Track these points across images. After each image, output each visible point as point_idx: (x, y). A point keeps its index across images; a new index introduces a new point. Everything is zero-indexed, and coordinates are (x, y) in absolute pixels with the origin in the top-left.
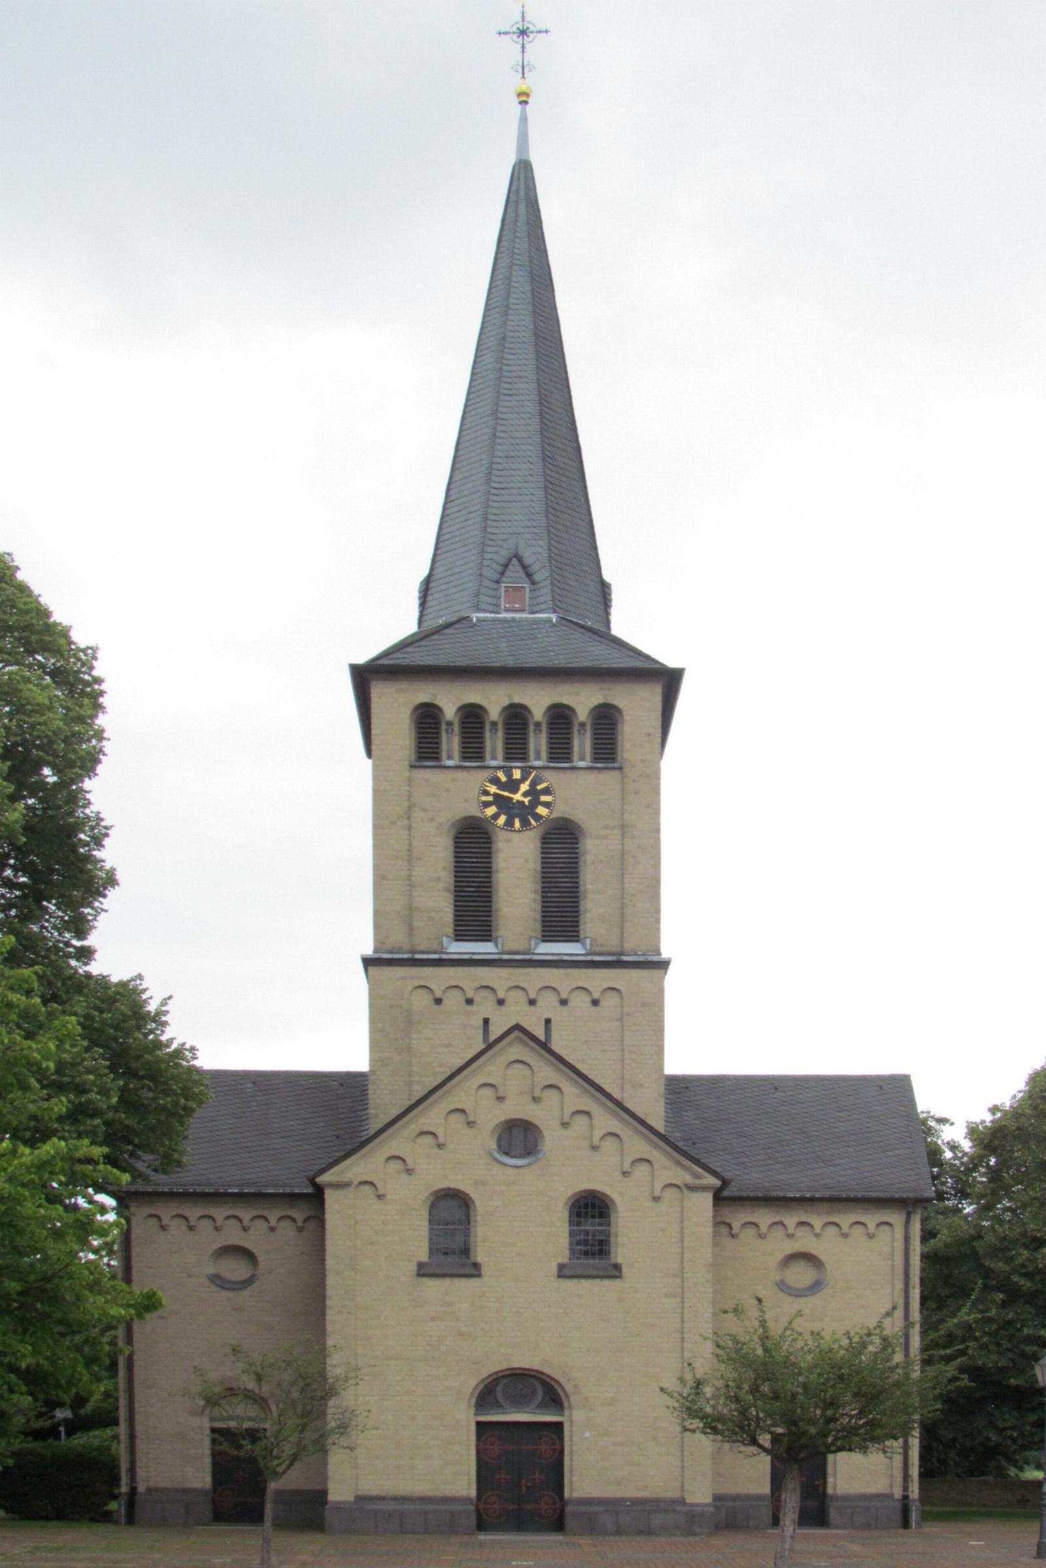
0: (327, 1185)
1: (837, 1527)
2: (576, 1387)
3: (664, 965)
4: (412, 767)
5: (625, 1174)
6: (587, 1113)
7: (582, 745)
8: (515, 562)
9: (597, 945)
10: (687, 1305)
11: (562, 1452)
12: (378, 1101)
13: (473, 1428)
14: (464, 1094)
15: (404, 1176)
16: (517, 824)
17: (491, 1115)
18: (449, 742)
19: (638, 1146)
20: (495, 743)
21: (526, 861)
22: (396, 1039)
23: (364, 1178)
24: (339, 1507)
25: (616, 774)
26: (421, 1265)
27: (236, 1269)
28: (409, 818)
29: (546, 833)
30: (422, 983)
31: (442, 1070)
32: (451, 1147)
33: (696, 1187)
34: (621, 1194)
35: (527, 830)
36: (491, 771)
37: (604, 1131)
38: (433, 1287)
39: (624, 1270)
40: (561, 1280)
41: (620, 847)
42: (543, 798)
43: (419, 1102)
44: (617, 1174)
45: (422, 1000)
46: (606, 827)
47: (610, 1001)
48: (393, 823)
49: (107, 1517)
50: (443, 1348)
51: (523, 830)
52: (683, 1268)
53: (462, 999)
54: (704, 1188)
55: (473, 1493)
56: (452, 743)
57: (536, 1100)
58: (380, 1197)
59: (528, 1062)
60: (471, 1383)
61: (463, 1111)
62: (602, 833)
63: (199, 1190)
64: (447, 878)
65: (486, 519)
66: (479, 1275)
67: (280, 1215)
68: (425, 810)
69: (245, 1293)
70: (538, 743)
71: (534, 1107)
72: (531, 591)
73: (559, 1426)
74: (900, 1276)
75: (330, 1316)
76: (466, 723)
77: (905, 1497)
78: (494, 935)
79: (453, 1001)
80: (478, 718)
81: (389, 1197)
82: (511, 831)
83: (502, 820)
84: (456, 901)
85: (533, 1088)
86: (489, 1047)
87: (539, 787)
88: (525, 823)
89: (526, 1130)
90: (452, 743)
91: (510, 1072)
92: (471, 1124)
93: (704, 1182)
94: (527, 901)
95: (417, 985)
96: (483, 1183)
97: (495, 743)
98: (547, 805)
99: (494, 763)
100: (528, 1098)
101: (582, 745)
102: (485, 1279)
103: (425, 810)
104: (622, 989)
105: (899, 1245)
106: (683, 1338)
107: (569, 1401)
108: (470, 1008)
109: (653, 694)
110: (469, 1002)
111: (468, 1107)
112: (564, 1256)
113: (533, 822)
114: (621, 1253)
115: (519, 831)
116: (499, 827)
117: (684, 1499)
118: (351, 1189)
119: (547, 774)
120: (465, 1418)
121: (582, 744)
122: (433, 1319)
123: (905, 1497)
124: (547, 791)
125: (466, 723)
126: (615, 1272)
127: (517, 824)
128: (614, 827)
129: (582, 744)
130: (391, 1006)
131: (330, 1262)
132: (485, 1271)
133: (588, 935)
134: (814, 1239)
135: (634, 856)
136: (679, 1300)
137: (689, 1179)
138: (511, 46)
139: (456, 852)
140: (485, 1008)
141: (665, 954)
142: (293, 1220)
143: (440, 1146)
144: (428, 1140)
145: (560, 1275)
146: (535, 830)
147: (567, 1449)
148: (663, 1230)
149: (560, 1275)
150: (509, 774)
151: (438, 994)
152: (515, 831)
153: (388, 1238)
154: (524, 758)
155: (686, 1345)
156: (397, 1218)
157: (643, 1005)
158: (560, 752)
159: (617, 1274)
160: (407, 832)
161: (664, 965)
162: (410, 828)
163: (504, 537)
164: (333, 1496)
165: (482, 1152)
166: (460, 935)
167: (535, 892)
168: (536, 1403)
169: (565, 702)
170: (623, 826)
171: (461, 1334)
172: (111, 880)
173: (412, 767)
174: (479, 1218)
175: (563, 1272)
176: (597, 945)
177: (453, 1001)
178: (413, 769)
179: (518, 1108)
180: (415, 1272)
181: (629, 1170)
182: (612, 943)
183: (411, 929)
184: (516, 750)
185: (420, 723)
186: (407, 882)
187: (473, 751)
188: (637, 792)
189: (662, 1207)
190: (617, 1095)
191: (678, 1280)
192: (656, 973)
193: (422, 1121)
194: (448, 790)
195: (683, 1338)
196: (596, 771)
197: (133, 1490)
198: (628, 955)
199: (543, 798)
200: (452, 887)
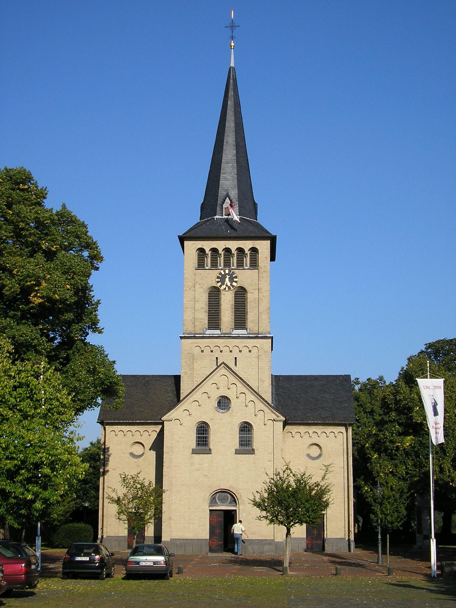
0: (165, 420)
2: (240, 496)
9: (251, 331)
12: (184, 388)
13: (209, 512)
14: (207, 386)
17: (216, 395)
19: (260, 405)
20: (221, 260)
21: (230, 301)
26: (193, 450)
31: (203, 376)
32: (203, 406)
33: (331, 424)
34: (255, 423)
38: (198, 457)
42: (235, 280)
43: (190, 393)
46: (253, 289)
47: (254, 351)
54: (280, 421)
55: (208, 537)
56: (208, 261)
62: (252, 291)
70: (234, 260)
71: (228, 391)
79: (207, 351)
81: (184, 424)
86: (218, 367)
87: (234, 276)
90: (208, 261)
91: (221, 378)
94: (230, 315)
96: (212, 419)
97: (221, 260)
98: (236, 282)
99: (220, 268)
102: (213, 455)
112: (237, 446)
114: (256, 445)
115: (227, 291)
119: (236, 271)
120: (206, 508)
121: (247, 260)
122: (196, 470)
124: (236, 277)
126: (252, 452)
128: (256, 289)
129: (247, 260)
130: (188, 353)
132: (212, 452)
133: (248, 327)
135: (262, 299)
137: (275, 417)
138: (229, 31)
140: (217, 354)
142: (157, 432)
150: (224, 271)
154: (230, 266)
157: (265, 352)
159: (253, 453)
165: (212, 408)
166: (210, 328)
167: (232, 312)
171: (205, 476)
174: (211, 432)
175: (237, 452)
176: (251, 331)
177: (207, 351)
180: (191, 453)
182: (255, 330)
186: (194, 309)
189: (267, 427)
190: (254, 386)
197: (102, 536)
198: (260, 334)
199: (235, 280)
200: (207, 311)
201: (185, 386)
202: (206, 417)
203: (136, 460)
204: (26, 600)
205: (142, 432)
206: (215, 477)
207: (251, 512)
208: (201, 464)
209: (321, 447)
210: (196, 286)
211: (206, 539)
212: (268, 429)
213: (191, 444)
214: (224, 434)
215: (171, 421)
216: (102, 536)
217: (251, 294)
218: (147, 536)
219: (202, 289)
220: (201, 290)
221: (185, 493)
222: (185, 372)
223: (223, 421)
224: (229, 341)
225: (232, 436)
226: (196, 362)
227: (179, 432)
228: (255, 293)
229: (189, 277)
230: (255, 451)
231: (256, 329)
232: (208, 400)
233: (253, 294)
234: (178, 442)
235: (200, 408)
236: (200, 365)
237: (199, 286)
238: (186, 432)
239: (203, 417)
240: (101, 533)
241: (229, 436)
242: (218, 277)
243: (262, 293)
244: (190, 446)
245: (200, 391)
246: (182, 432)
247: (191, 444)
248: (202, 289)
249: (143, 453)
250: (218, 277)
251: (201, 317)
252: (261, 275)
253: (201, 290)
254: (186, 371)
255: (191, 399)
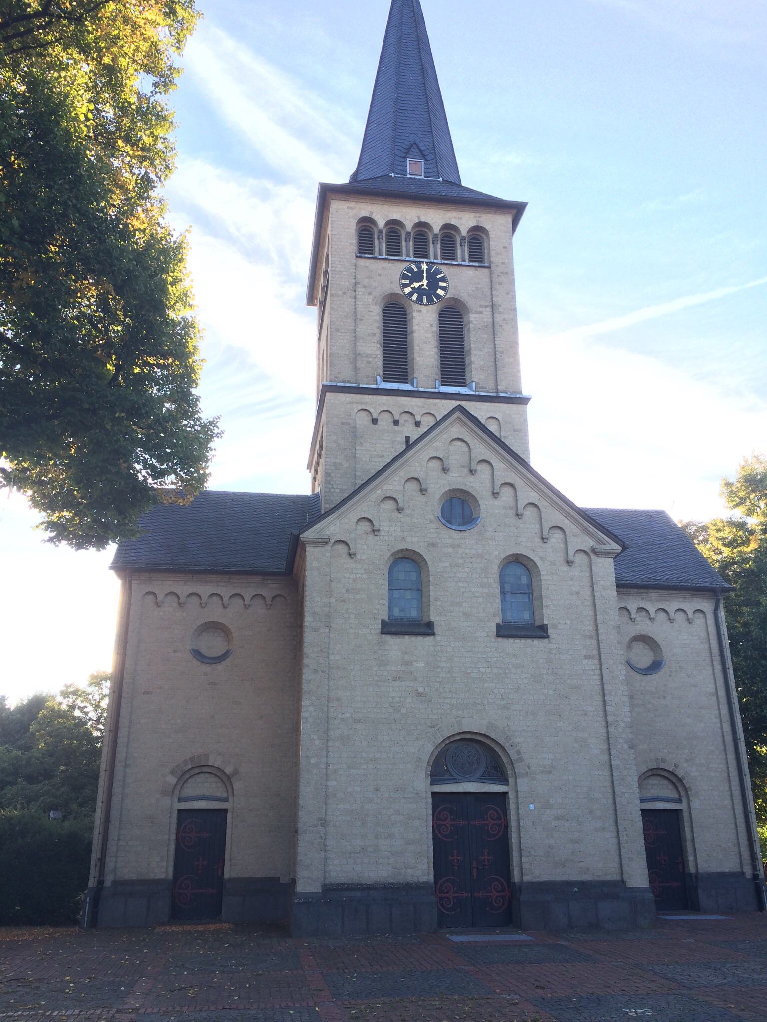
1: (705, 912)
2: (519, 752)
3: (523, 401)
4: (357, 257)
5: (544, 539)
6: (511, 485)
7: (463, 251)
8: (415, 146)
10: (604, 666)
11: (507, 827)
15: (371, 537)
16: (425, 301)
17: (439, 485)
18: (380, 244)
21: (432, 326)
22: (345, 449)
23: (339, 538)
24: (309, 901)
25: (486, 271)
27: (213, 645)
28: (355, 291)
29: (442, 311)
30: (364, 407)
32: (408, 512)
34: (542, 558)
35: (431, 304)
36: (408, 264)
37: (526, 501)
39: (550, 631)
40: (500, 639)
41: (491, 320)
42: (441, 284)
44: (537, 540)
45: (362, 420)
46: (482, 306)
48: (344, 293)
49: (70, 920)
50: (404, 711)
51: (429, 305)
52: (597, 630)
53: (391, 420)
54: (607, 554)
55: (431, 878)
57: (472, 472)
58: (351, 555)
59: (466, 440)
60: (427, 748)
61: (417, 479)
62: (480, 310)
63: (191, 568)
64: (379, 336)
65: (396, 125)
66: (433, 634)
67: (255, 593)
68: (365, 287)
69: (220, 667)
71: (471, 478)
72: (425, 164)
73: (505, 795)
74: (717, 659)
75: (307, 675)
76: (390, 235)
77: (755, 877)
78: (410, 378)
79: (385, 422)
80: (396, 232)
81: (358, 556)
82: (421, 305)
83: (415, 297)
84: (384, 353)
85: (470, 463)
88: (430, 301)
89: (463, 501)
91: (452, 448)
92: (423, 491)
93: (607, 547)
94: (433, 353)
95: (360, 408)
97: (408, 247)
98: (444, 289)
100: (466, 470)
101: (463, 251)
102: (438, 638)
103: (365, 287)
104: (500, 418)
105: (712, 629)
106: (604, 701)
107: (513, 769)
108: (396, 428)
109: (507, 219)
110: (396, 423)
111: (421, 475)
113: (435, 300)
115: (426, 305)
116: (413, 302)
117: (623, 881)
118: (328, 548)
120: (423, 786)
121: (463, 252)
122: (395, 679)
123: (755, 877)
124: (444, 280)
125: (390, 235)
127: (425, 301)
128: (486, 307)
129: (463, 252)
130: (342, 423)
131: (308, 619)
132: (437, 629)
134: (649, 622)
136: (596, 662)
139: (384, 320)
141: (525, 393)
143: (399, 510)
144: (390, 504)
145: (499, 635)
146: (436, 305)
147: (513, 824)
148: (577, 593)
149: (499, 635)
151: (375, 416)
152: (423, 305)
153: (358, 596)
155: (608, 708)
156: (364, 576)
158: (449, 254)
160: (353, 301)
161: (524, 401)
162: (355, 298)
163: (408, 135)
164: (300, 888)
166: (386, 379)
168: (478, 775)
169: (453, 223)
170: (493, 306)
171: (420, 695)
172: (111, 568)
173: (357, 257)
177: (385, 422)
178: (357, 259)
179: (457, 479)
180: (379, 631)
181: (547, 536)
183: (356, 369)
184: (421, 251)
185: (360, 233)
187: (394, 249)
188: (500, 284)
189: (575, 572)
191: (594, 642)
192: (521, 407)
193: (386, 487)
194: (380, 275)
195: (604, 701)
196: (474, 269)
197: (101, 882)
199: (441, 284)
201: (334, 494)
202: (416, 540)
203: (207, 668)
204: (437, 381)
205: (226, 600)
206: (445, 698)
207: (552, 801)
208: (407, 663)
209: (659, 643)
210: (358, 290)
211: (427, 883)
212: (577, 574)
213: (379, 607)
214: (466, 585)
215: (326, 543)
216: (101, 882)
217: (477, 316)
218: (230, 880)
219: (371, 297)
220: (369, 299)
221: (364, 743)
222: (334, 463)
223: (461, 551)
224: (435, 405)
225: (486, 590)
226: (361, 444)
227: (347, 576)
228: (485, 313)
229: (342, 270)
230: (550, 631)
231: (491, 384)
232: (422, 499)
233: (481, 316)
234: (344, 601)
235: (399, 515)
236: (370, 451)
237: (363, 290)
238: (364, 576)
239: (409, 539)
240: (97, 874)
241: (479, 590)
242: (404, 277)
243: (500, 313)
244: (376, 612)
245: (402, 473)
246: (353, 576)
247: (379, 607)
248: (371, 297)
249: (228, 652)
250: (404, 277)
251: (369, 352)
252: (496, 280)
253: (369, 299)
254: (339, 461)
255: (379, 491)
